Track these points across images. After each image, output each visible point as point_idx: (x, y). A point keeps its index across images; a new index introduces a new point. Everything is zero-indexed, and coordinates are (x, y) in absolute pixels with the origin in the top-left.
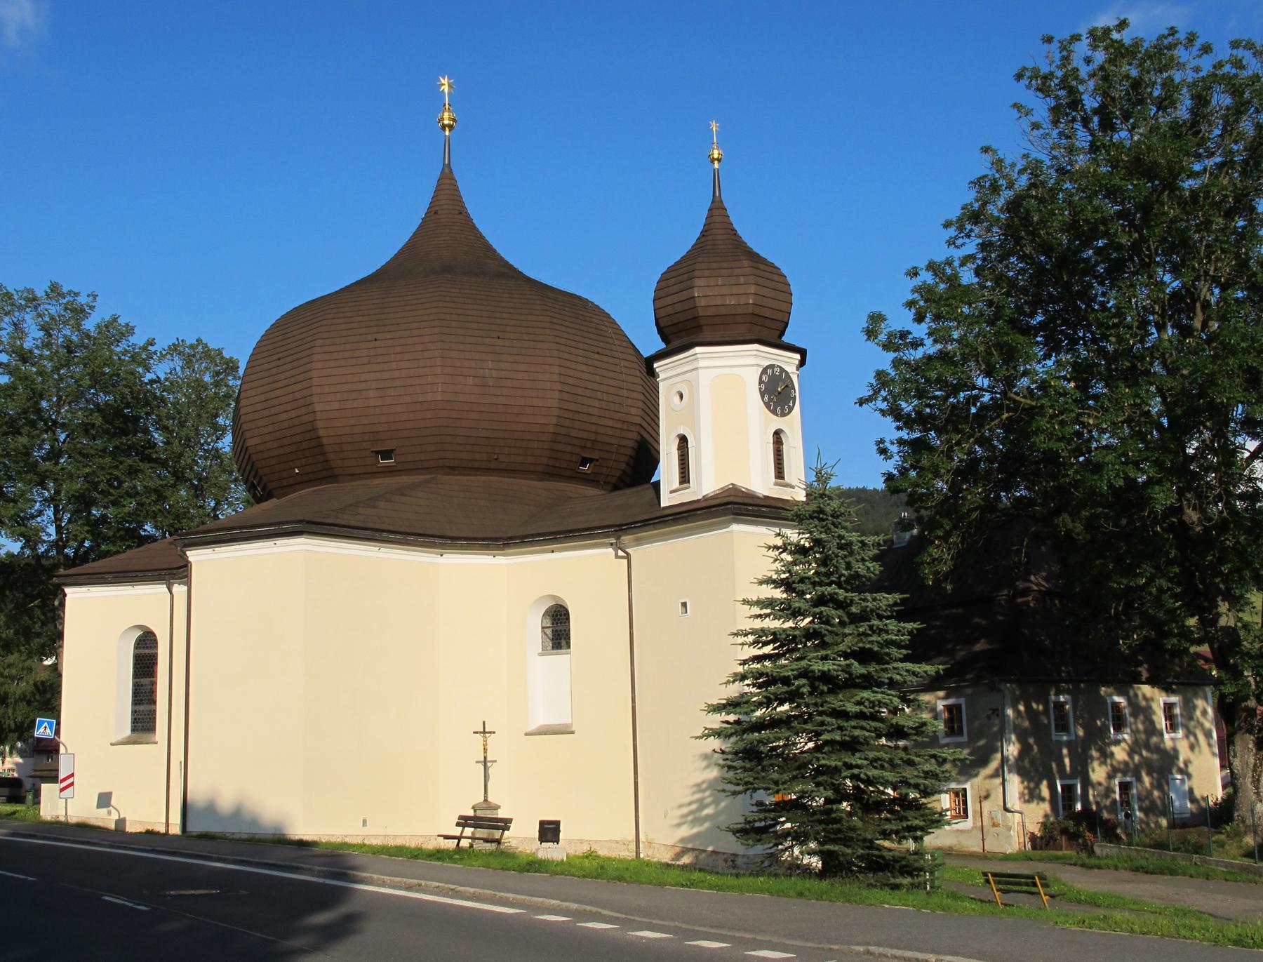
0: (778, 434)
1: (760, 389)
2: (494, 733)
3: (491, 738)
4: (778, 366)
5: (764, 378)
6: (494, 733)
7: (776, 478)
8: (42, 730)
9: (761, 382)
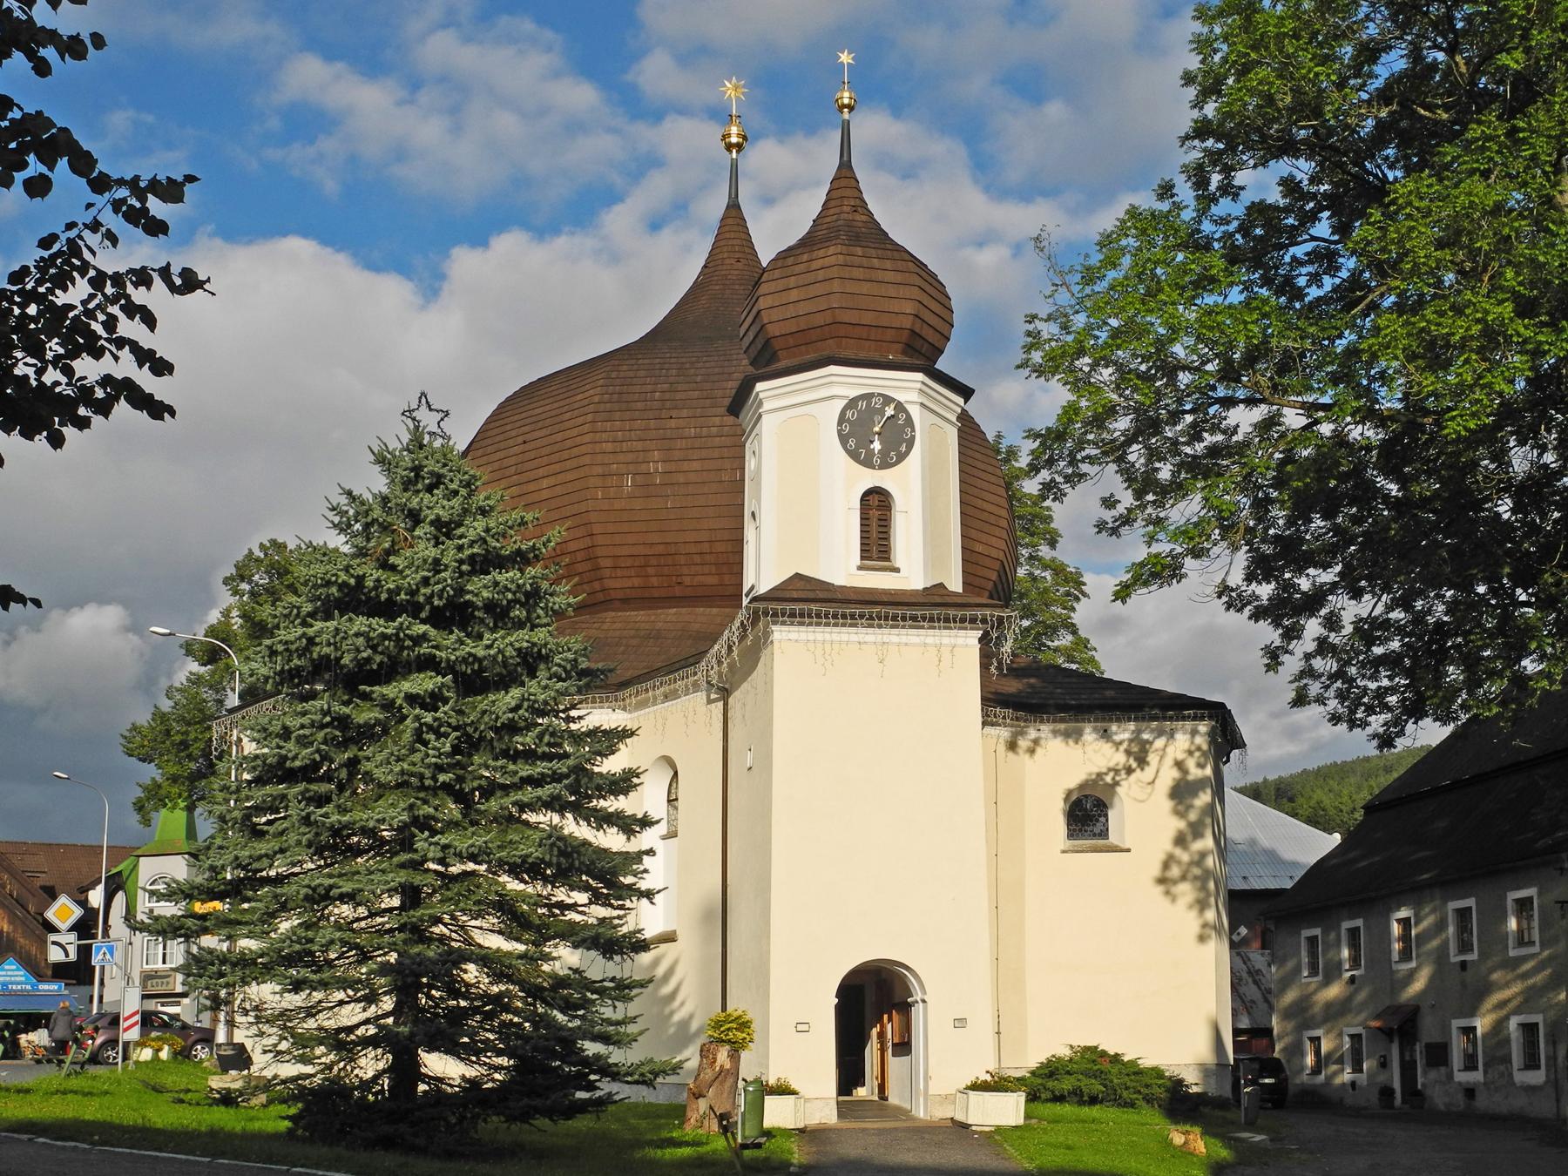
0: (876, 507)
1: (839, 432)
4: (879, 395)
5: (849, 414)
7: (862, 558)
8: (100, 957)
9: (842, 419)
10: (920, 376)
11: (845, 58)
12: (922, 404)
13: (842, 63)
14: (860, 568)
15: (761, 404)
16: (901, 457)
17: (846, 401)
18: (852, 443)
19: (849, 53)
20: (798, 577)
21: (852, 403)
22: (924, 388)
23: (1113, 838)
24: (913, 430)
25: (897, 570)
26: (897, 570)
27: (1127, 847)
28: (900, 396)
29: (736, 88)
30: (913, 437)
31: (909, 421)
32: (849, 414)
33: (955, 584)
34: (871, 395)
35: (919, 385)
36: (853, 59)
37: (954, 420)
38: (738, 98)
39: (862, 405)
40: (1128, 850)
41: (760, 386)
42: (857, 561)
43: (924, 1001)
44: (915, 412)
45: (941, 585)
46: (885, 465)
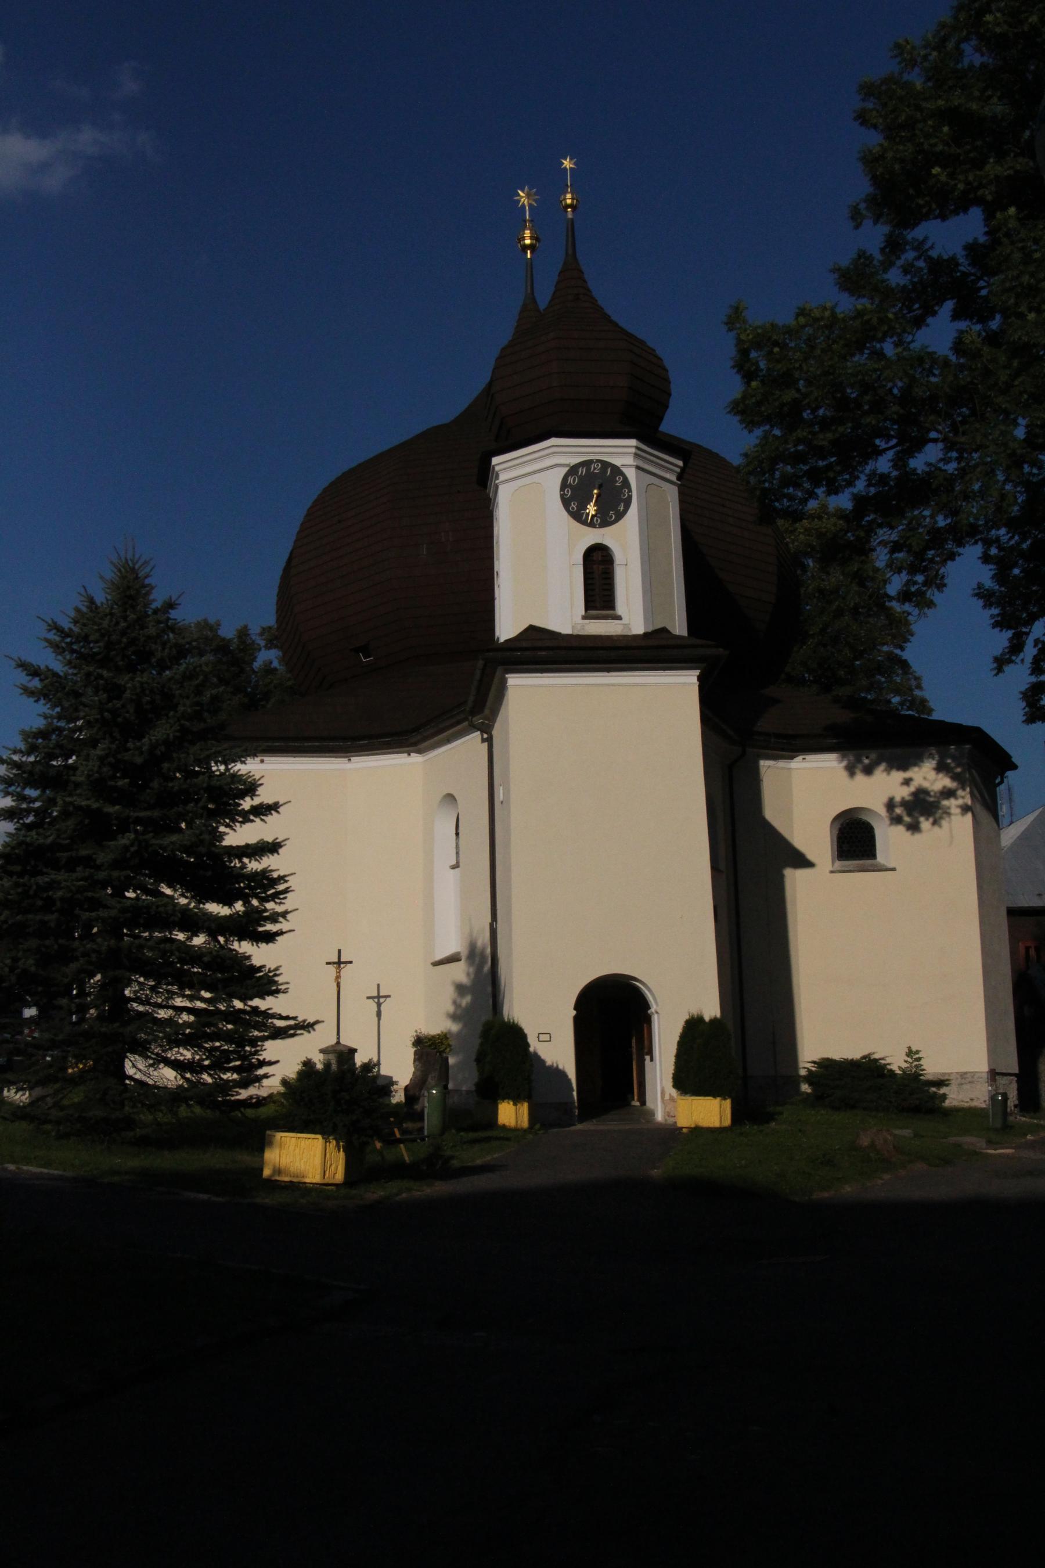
1: (562, 497)
2: (351, 962)
3: (346, 971)
4: (598, 461)
5: (570, 480)
6: (351, 962)
7: (587, 608)
10: (633, 442)
11: (567, 163)
12: (638, 468)
13: (565, 168)
14: (584, 618)
15: (497, 477)
16: (620, 516)
17: (567, 469)
18: (574, 506)
19: (571, 159)
20: (532, 629)
21: (573, 470)
22: (639, 452)
23: (881, 858)
24: (630, 490)
25: (619, 618)
26: (619, 618)
27: (890, 865)
28: (617, 461)
29: (528, 196)
30: (630, 498)
31: (626, 483)
32: (570, 480)
33: (679, 627)
34: (591, 462)
35: (633, 450)
36: (575, 164)
37: (673, 478)
38: (530, 205)
39: (582, 471)
40: (894, 869)
41: (495, 460)
42: (583, 613)
43: (657, 1012)
44: (631, 474)
45: (664, 630)
46: (605, 523)
